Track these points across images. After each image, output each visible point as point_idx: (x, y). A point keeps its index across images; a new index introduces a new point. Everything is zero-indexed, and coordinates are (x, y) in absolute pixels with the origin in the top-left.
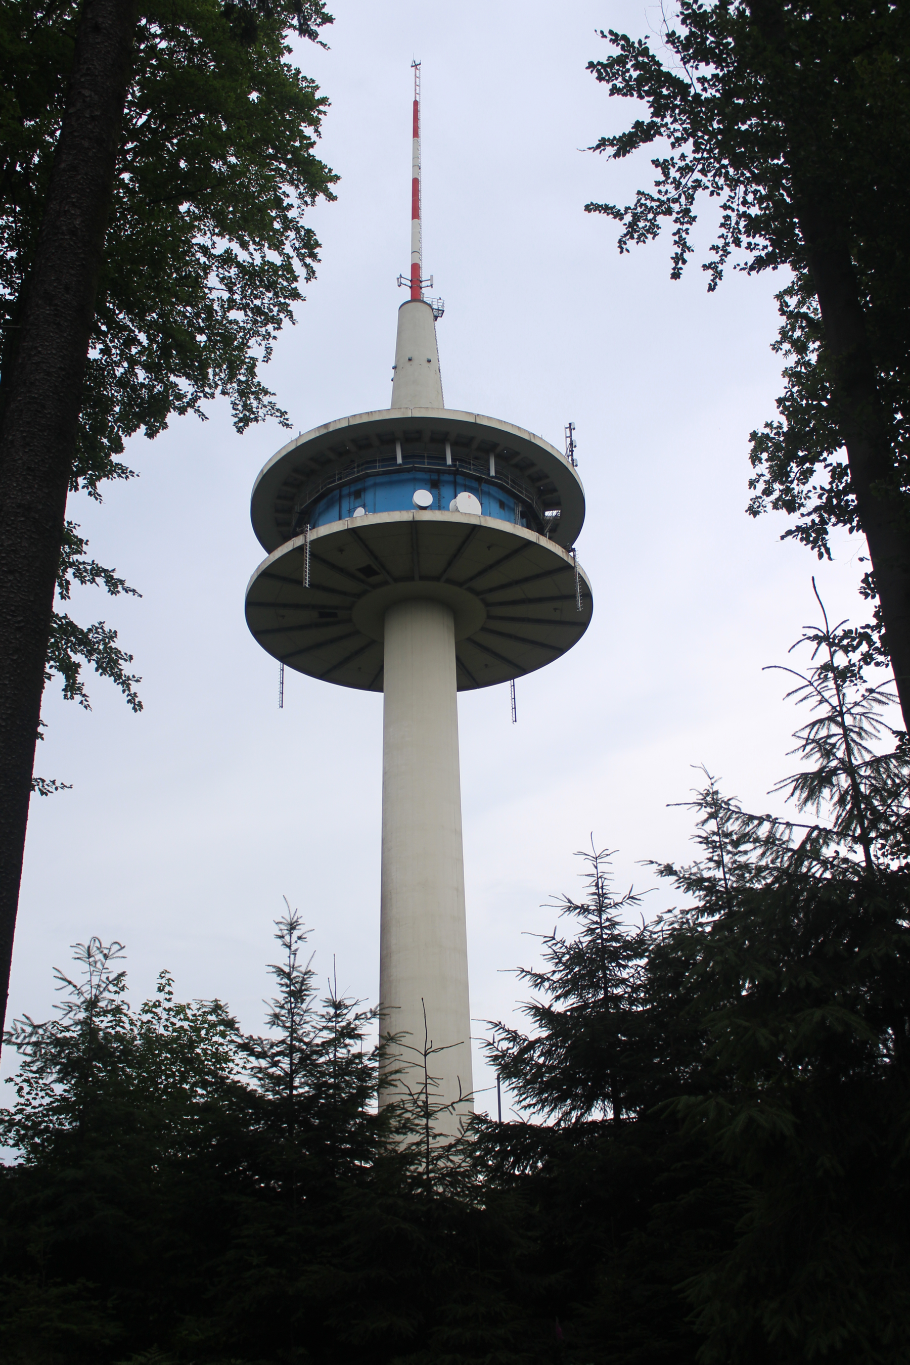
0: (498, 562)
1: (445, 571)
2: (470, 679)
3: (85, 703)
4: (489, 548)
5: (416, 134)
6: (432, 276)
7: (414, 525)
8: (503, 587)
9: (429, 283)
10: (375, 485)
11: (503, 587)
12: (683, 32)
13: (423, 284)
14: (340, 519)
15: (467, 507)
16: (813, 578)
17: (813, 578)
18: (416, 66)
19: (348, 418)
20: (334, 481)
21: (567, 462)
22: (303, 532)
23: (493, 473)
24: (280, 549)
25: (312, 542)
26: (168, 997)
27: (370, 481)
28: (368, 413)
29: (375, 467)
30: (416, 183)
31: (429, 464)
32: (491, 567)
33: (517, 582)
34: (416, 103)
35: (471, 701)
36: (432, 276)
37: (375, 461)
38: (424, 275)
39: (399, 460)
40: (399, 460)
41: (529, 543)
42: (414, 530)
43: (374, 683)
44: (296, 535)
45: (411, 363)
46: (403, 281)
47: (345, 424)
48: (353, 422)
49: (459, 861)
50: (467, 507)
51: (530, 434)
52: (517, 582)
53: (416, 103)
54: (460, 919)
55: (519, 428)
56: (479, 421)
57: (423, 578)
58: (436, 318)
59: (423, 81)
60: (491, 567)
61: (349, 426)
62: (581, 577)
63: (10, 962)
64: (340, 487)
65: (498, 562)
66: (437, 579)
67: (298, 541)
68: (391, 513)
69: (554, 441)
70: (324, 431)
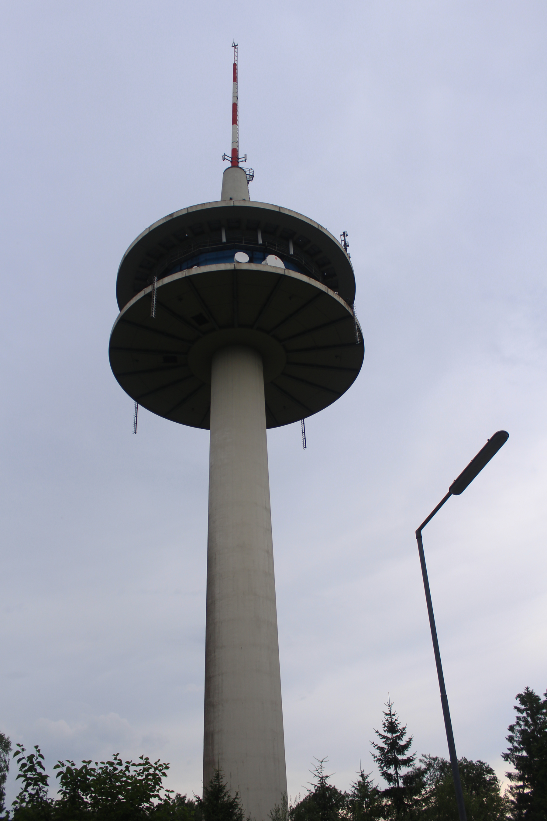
2: (275, 420)
6: (246, 155)
7: (235, 272)
9: (244, 159)
13: (240, 160)
15: (274, 263)
16: (499, 439)
17: (499, 439)
18: (235, 46)
19: (187, 208)
21: (343, 250)
22: (152, 283)
23: (292, 252)
24: (135, 298)
25: (158, 289)
26: (20, 756)
28: (202, 204)
30: (235, 106)
31: (245, 243)
34: (235, 65)
35: (273, 434)
36: (246, 155)
38: (241, 155)
42: (237, 274)
43: (201, 420)
44: (146, 286)
46: (226, 157)
47: (185, 212)
48: (190, 211)
49: (269, 531)
50: (274, 263)
51: (318, 225)
54: (270, 574)
55: (311, 219)
56: (282, 211)
58: (248, 181)
62: (358, 326)
67: (148, 290)
68: (218, 265)
69: (335, 234)
70: (170, 218)
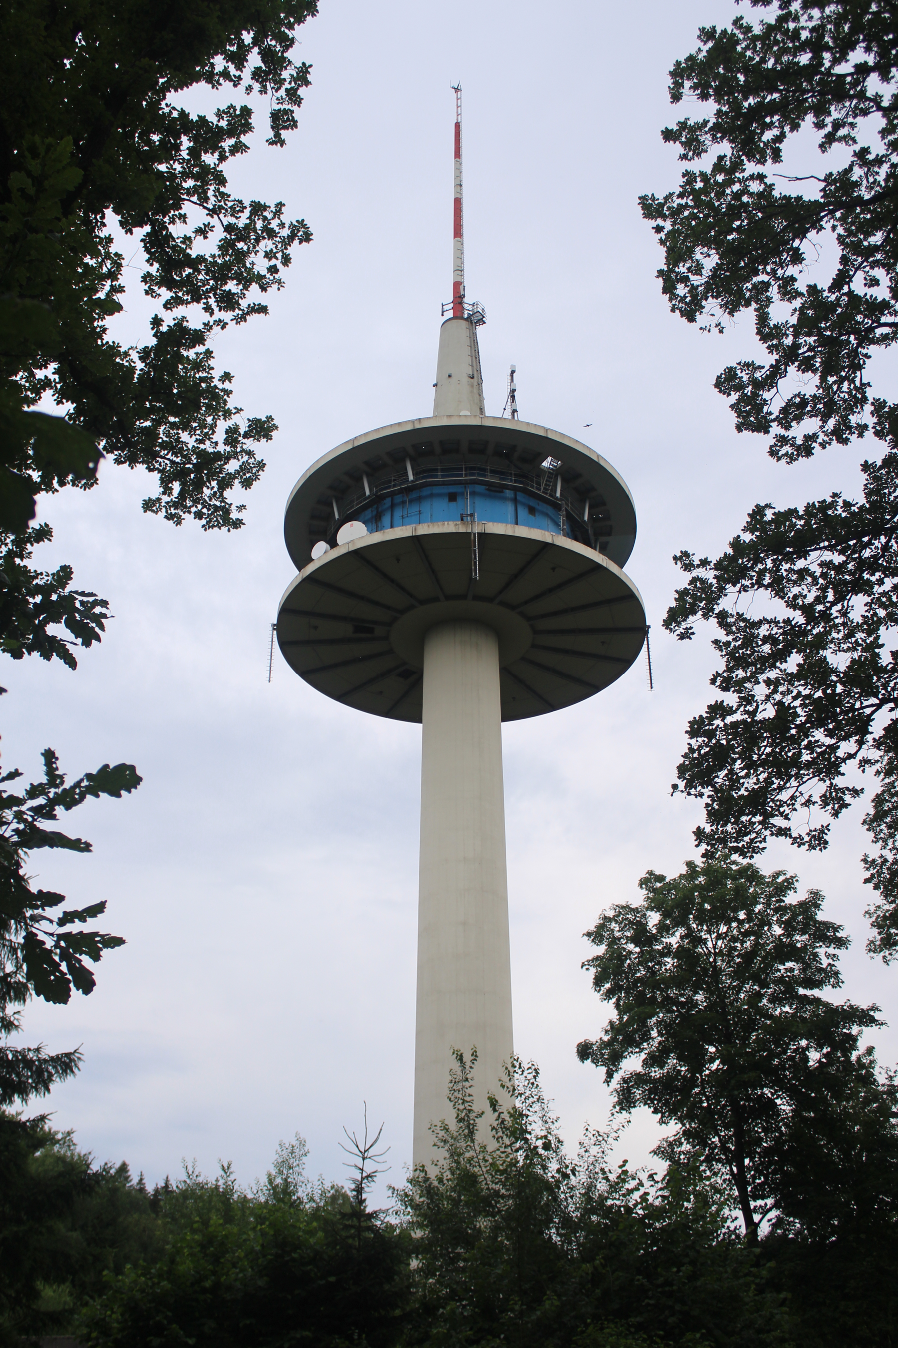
0: (560, 586)
1: (501, 592)
3: (614, 1135)
4: (553, 569)
5: (458, 154)
8: (555, 613)
10: (431, 496)
11: (555, 613)
12: (672, 86)
14: (392, 527)
18: (457, 90)
19: (413, 422)
20: (390, 487)
27: (426, 491)
29: (436, 477)
30: (458, 202)
32: (551, 590)
33: (573, 609)
34: (458, 126)
37: (436, 470)
39: (411, 478)
40: (411, 478)
41: (599, 567)
45: (450, 380)
52: (573, 609)
53: (458, 126)
57: (477, 598)
59: (464, 102)
60: (551, 590)
61: (353, 448)
63: (55, 893)
64: (392, 494)
65: (560, 586)
66: (490, 600)
